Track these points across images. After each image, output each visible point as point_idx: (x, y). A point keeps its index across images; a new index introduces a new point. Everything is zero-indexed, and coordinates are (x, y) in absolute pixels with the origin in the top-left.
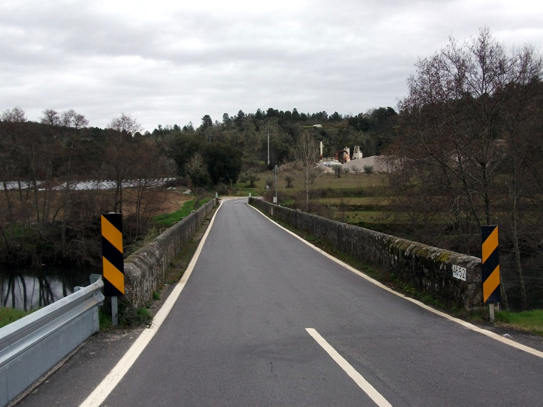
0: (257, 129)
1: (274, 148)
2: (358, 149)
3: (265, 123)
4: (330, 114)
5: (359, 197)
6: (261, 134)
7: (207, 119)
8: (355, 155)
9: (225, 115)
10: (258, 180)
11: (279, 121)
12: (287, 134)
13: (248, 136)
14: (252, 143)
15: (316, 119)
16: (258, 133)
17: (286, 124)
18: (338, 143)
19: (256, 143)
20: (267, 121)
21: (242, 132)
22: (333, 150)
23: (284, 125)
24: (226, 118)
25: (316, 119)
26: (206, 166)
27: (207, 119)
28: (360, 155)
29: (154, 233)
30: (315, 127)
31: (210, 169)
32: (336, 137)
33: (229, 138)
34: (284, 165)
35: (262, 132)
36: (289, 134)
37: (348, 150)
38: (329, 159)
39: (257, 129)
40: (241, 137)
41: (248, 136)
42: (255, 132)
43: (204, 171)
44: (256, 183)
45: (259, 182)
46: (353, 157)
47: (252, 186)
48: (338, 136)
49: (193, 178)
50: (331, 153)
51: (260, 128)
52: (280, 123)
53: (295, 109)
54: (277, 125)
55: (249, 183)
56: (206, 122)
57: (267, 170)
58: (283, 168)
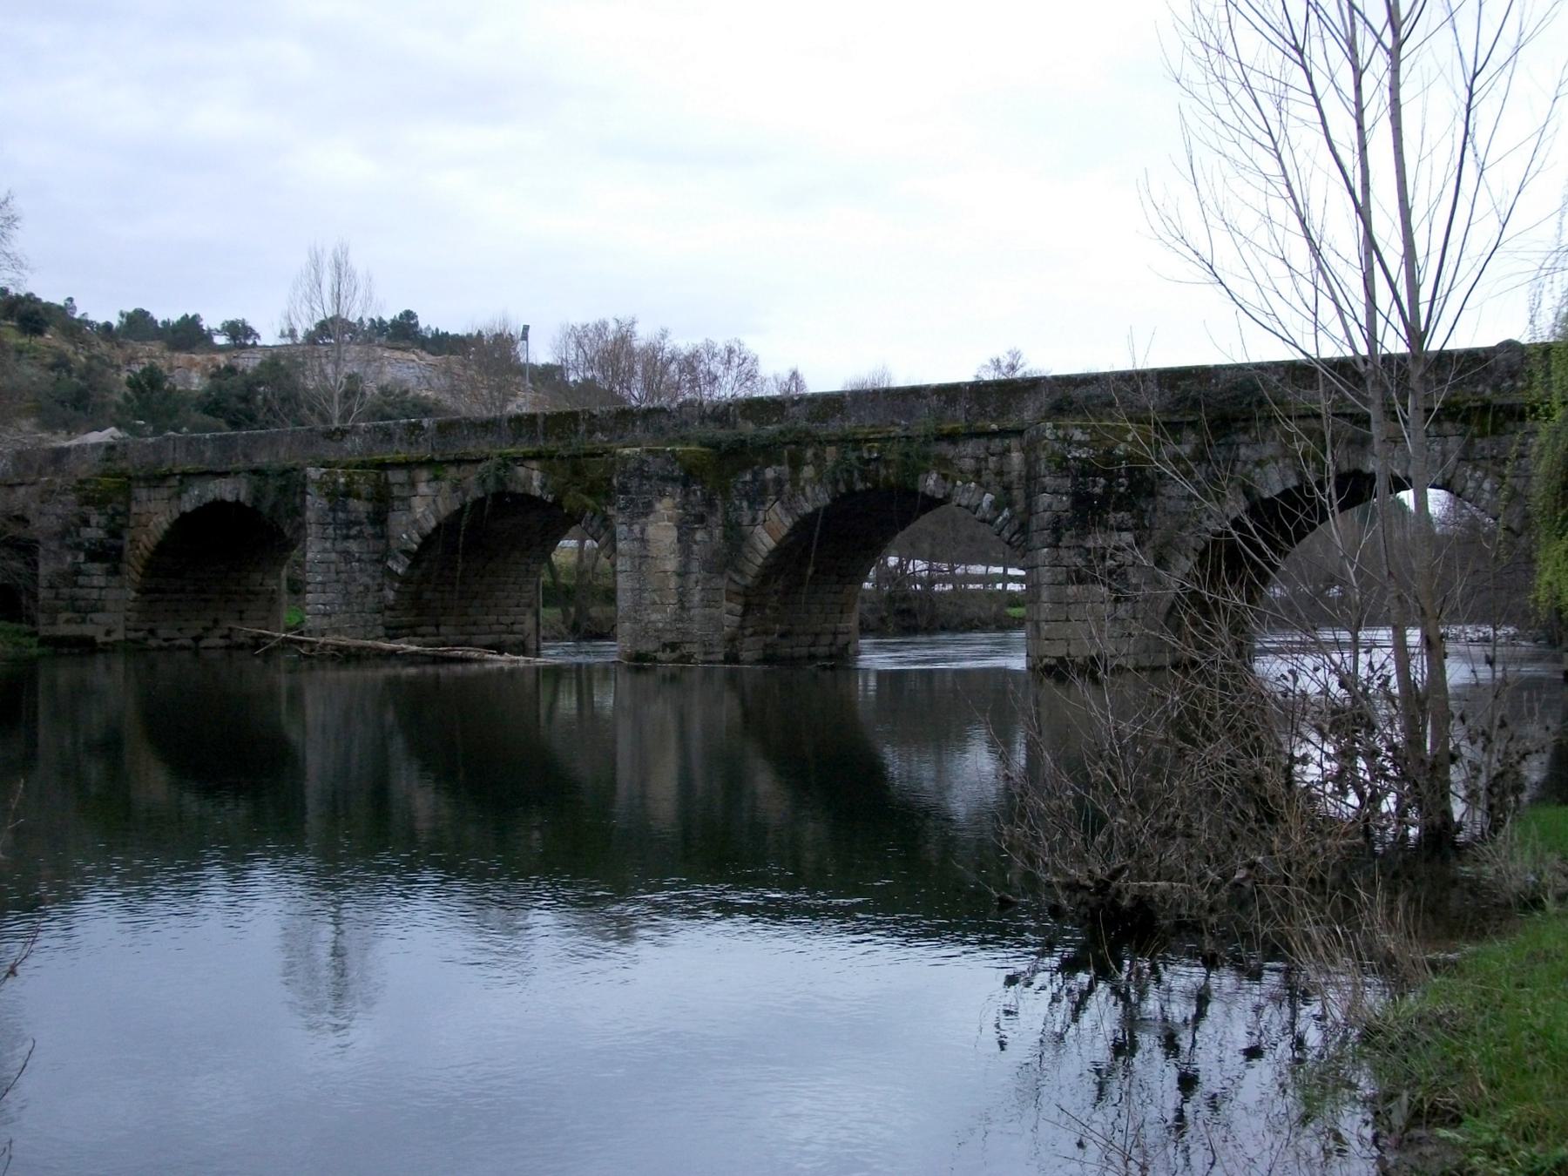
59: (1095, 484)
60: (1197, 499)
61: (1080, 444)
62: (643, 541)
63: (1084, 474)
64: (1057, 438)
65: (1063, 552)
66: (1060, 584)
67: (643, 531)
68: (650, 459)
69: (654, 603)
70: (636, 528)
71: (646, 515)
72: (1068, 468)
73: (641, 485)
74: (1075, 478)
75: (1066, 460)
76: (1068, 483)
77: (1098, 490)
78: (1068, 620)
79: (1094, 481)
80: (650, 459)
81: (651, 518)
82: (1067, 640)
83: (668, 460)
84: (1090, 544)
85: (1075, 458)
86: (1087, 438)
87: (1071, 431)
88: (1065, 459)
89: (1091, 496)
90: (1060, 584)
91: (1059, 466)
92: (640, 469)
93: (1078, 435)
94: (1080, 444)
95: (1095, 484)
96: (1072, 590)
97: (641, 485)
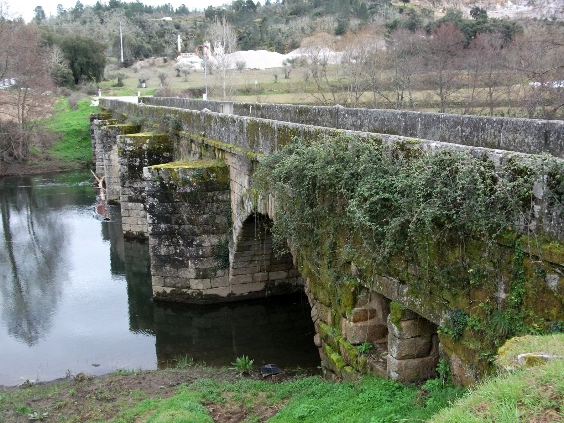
0: (102, 22)
1: (128, 44)
2: (218, 43)
3: (110, 15)
4: (176, 6)
5: (247, 95)
6: (108, 28)
7: (40, 12)
8: (216, 51)
9: (60, 7)
10: (127, 77)
11: (126, 13)
12: (137, 27)
13: (93, 30)
14: (98, 38)
15: (162, 12)
16: (103, 26)
17: (134, 16)
18: (196, 37)
19: (102, 38)
20: (112, 12)
21: (85, 25)
22: (191, 45)
23: (132, 17)
24: (60, 9)
25: (162, 12)
26: (67, 62)
27: (40, 12)
28: (220, 50)
29: (392, 180)
30: (164, 20)
31: (72, 66)
32: (192, 31)
33: (71, 31)
34: (140, 62)
35: (109, 25)
36: (140, 27)
37: (209, 45)
38: (188, 54)
39: (102, 22)
40: (84, 31)
41: (93, 30)
42: (100, 25)
43: (65, 69)
44: (124, 81)
45: (127, 80)
46: (214, 53)
47: (120, 85)
48: (194, 30)
49: (54, 75)
50: (189, 49)
51: (105, 20)
52: (127, 15)
53: (39, 7)
54: (125, 17)
55: (116, 81)
56: (38, 14)
57: (121, 67)
58: (140, 65)
59: (136, 161)
60: (296, 132)
61: (130, 145)
62: (109, 160)
63: (132, 157)
64: (121, 142)
65: (126, 189)
66: (125, 202)
67: (109, 156)
68: (110, 130)
69: (115, 182)
70: (107, 155)
71: (110, 151)
72: (126, 155)
73: (107, 140)
74: (129, 159)
75: (125, 151)
76: (126, 160)
77: (137, 164)
78: (129, 216)
79: (135, 160)
80: (110, 130)
81: (112, 152)
82: (130, 224)
83: (117, 130)
84: (135, 186)
85: (128, 150)
86: (132, 142)
87: (126, 139)
88: (125, 151)
89: (134, 166)
90: (125, 202)
91: (123, 154)
92: (107, 134)
93: (129, 141)
94: (130, 145)
95: (136, 161)
96: (130, 204)
97: (107, 140)
